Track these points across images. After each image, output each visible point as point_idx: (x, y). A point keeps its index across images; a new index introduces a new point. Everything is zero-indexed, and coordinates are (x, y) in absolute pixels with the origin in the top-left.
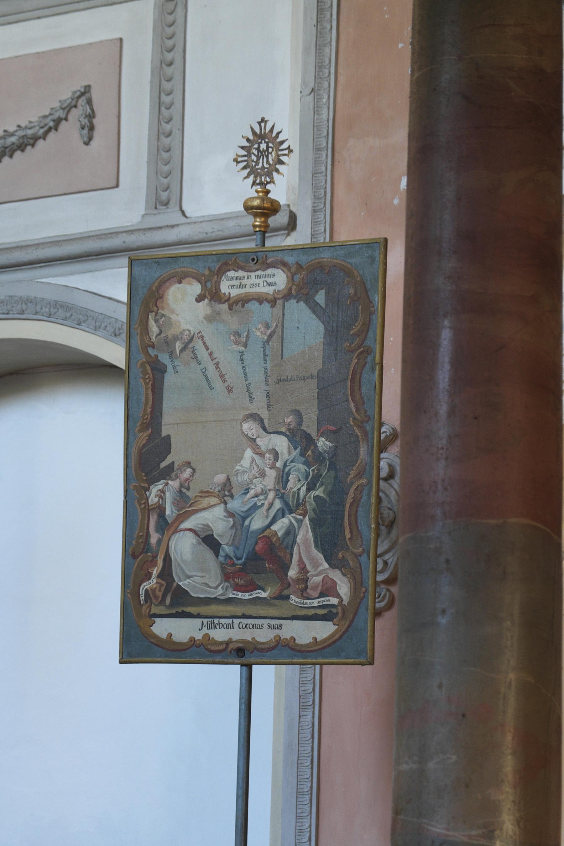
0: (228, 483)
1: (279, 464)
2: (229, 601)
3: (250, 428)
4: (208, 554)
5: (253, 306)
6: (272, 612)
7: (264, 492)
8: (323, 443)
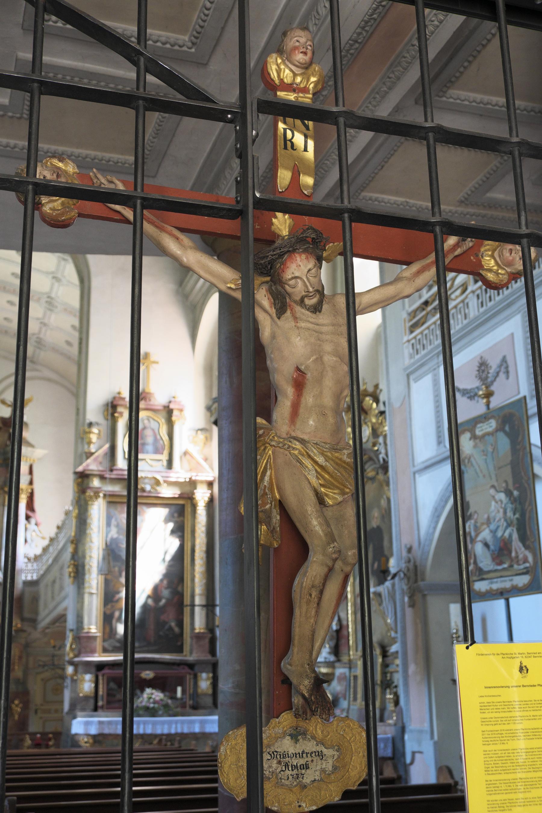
0: (488, 519)
1: (503, 506)
2: (496, 571)
3: (492, 491)
4: (486, 549)
5: (487, 438)
6: (509, 573)
7: (500, 520)
8: (516, 493)
